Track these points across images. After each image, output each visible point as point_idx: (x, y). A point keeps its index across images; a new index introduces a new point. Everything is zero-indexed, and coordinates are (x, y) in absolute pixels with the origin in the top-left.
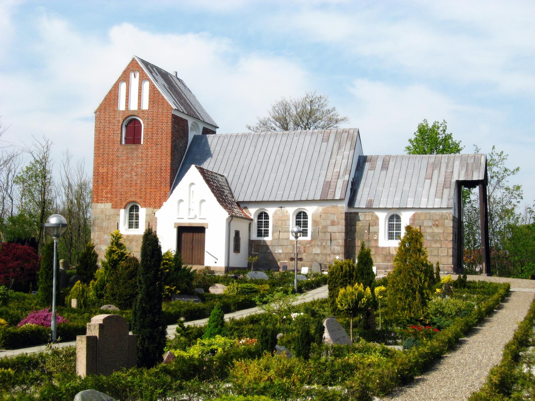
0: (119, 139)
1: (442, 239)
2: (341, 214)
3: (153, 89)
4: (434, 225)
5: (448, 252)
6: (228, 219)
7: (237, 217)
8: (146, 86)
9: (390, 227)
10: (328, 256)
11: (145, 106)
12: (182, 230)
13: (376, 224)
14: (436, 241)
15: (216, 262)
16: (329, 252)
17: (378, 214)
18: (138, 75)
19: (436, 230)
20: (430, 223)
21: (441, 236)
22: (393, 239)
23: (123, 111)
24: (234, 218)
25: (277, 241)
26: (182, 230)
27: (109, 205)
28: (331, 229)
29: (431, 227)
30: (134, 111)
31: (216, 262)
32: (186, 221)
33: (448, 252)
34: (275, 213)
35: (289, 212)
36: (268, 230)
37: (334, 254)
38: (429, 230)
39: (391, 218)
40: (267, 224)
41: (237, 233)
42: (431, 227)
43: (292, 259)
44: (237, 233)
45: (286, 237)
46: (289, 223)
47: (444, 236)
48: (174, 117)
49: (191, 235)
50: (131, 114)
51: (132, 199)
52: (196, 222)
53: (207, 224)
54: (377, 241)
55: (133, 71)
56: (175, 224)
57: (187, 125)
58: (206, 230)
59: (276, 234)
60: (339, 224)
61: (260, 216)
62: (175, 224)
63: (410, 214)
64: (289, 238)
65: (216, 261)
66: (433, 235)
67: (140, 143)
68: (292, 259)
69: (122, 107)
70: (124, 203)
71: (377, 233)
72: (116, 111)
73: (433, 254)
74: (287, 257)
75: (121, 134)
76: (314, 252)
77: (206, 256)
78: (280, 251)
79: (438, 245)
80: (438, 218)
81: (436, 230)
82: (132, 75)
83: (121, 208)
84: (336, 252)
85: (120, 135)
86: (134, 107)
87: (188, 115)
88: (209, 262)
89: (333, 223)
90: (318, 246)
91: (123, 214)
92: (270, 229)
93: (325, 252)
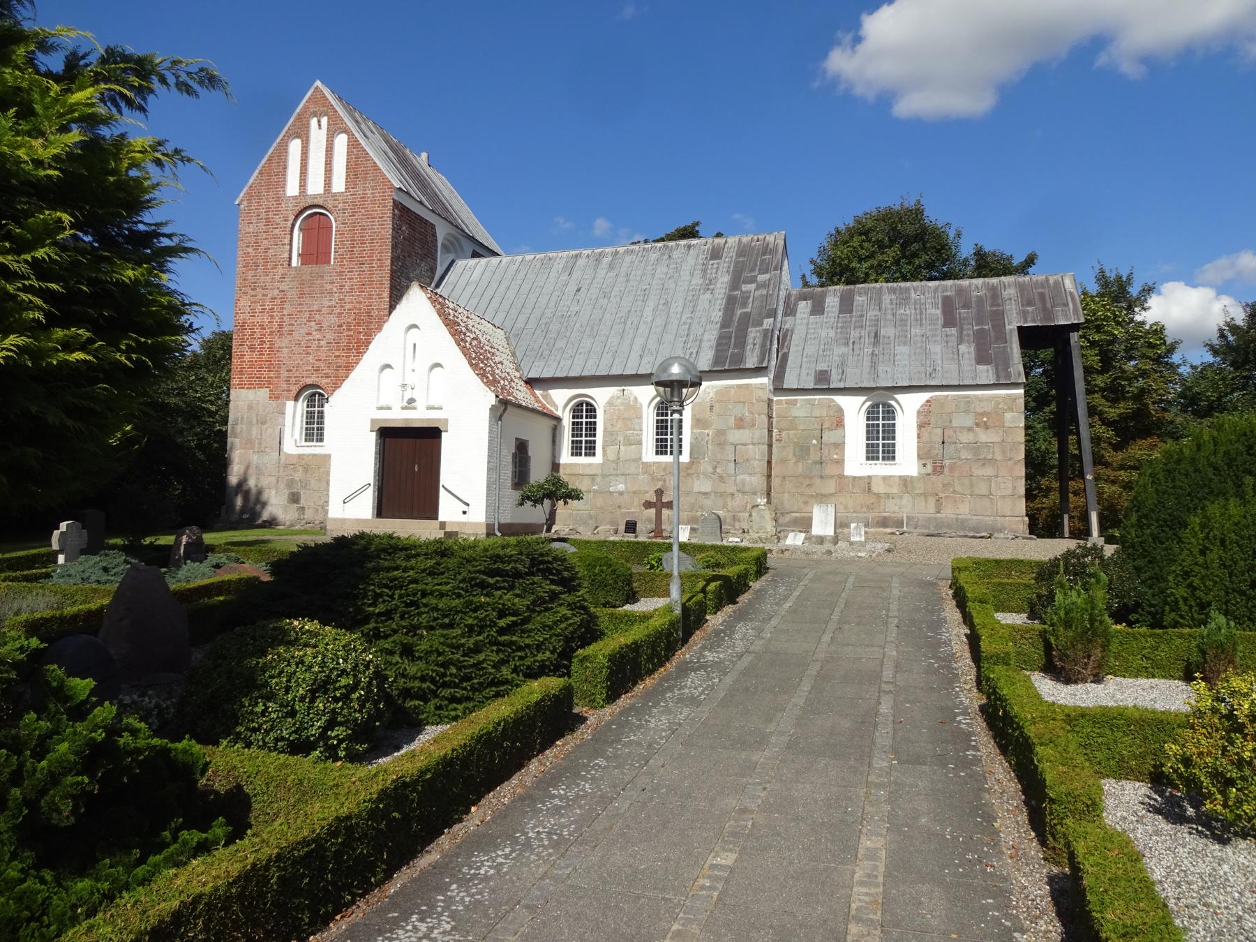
0: (286, 255)
1: (998, 456)
2: (758, 401)
3: (353, 144)
4: (978, 425)
5: (1014, 488)
6: (493, 409)
7: (520, 406)
8: (341, 141)
9: (871, 432)
10: (729, 499)
11: (339, 185)
12: (389, 436)
13: (839, 423)
14: (985, 462)
15: (464, 513)
16: (732, 489)
17: (841, 400)
18: (324, 120)
19: (984, 437)
20: (968, 421)
21: (997, 450)
22: (878, 459)
23: (295, 198)
24: (510, 409)
25: (614, 465)
26: (389, 436)
27: (263, 393)
28: (736, 436)
29: (970, 429)
30: (315, 196)
31: (464, 513)
32: (398, 416)
33: (1014, 488)
34: (610, 403)
35: (640, 400)
36: (594, 442)
37: (744, 493)
38: (966, 438)
39: (871, 414)
40: (592, 428)
41: (522, 448)
42: (970, 429)
43: (648, 505)
44: (522, 448)
45: (634, 457)
46: (640, 424)
47: (1004, 452)
48: (397, 205)
49: (408, 456)
50: (310, 202)
51: (309, 381)
52: (419, 416)
53: (446, 420)
54: (840, 462)
55: (314, 114)
56: (373, 421)
57: (434, 235)
58: (443, 434)
59: (612, 450)
60: (754, 425)
61: (577, 412)
62: (373, 421)
63: (921, 398)
64: (640, 458)
65: (465, 508)
66: (976, 448)
67: (329, 262)
68: (648, 505)
69: (292, 189)
70: (295, 389)
71: (840, 446)
72: (279, 198)
73: (977, 492)
74: (636, 500)
75: (291, 245)
76: (696, 489)
77: (444, 499)
78: (621, 487)
79: (989, 471)
80: (988, 407)
81: (984, 437)
82: (314, 122)
83: (288, 399)
84: (747, 488)
85: (288, 247)
86: (315, 187)
87: (433, 211)
88: (448, 510)
89: (740, 424)
90: (706, 476)
91: (295, 412)
92: (599, 439)
93: (722, 488)
